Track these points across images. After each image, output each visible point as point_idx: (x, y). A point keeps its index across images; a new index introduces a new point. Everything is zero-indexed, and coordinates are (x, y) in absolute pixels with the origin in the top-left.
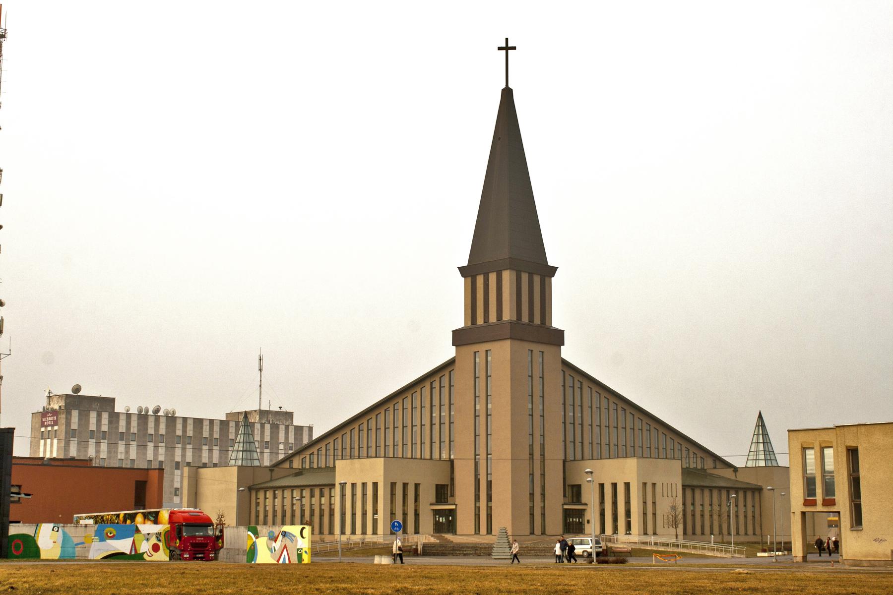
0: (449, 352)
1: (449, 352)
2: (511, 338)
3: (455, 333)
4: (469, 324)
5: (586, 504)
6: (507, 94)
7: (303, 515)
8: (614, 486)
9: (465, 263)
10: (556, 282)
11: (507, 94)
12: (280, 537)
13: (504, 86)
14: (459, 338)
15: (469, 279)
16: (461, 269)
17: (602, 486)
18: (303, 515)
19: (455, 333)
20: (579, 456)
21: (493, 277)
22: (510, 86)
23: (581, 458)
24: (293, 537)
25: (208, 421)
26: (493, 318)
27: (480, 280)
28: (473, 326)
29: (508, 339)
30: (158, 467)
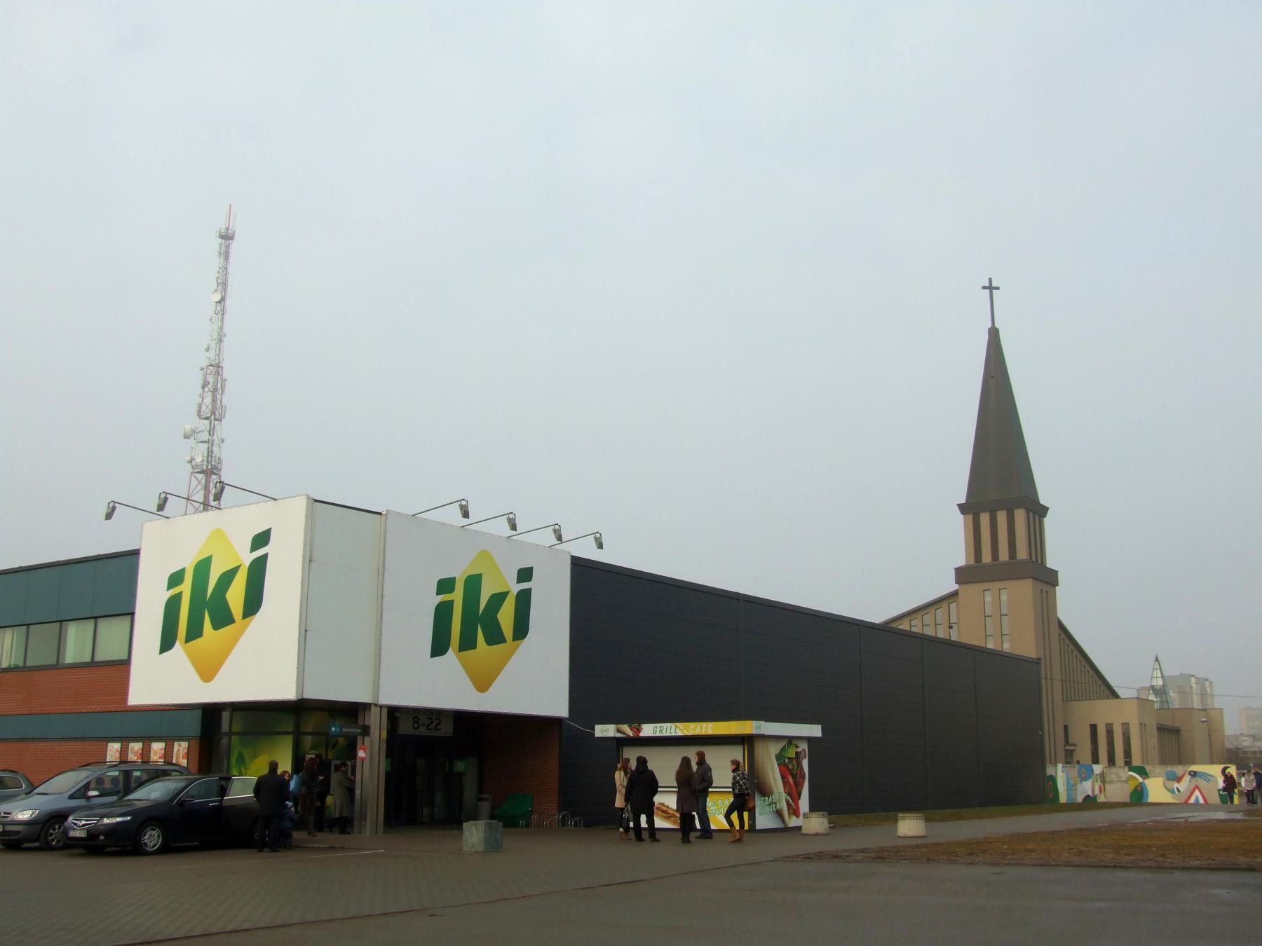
0: (951, 586)
1: (951, 586)
2: (1034, 578)
3: (958, 570)
4: (972, 562)
5: (1075, 745)
6: (994, 334)
7: (1128, 753)
8: (1110, 732)
9: (963, 501)
10: (1048, 521)
11: (994, 334)
12: (1187, 778)
13: (990, 325)
14: (963, 575)
15: (970, 517)
16: (960, 506)
17: (1094, 728)
18: (1128, 753)
19: (958, 570)
20: (1069, 699)
21: (1002, 516)
22: (996, 326)
23: (383, 708)
24: (1209, 777)
25: (121, 655)
26: (1004, 555)
27: (985, 519)
28: (996, 563)
29: (1029, 578)
30: (1136, 696)
